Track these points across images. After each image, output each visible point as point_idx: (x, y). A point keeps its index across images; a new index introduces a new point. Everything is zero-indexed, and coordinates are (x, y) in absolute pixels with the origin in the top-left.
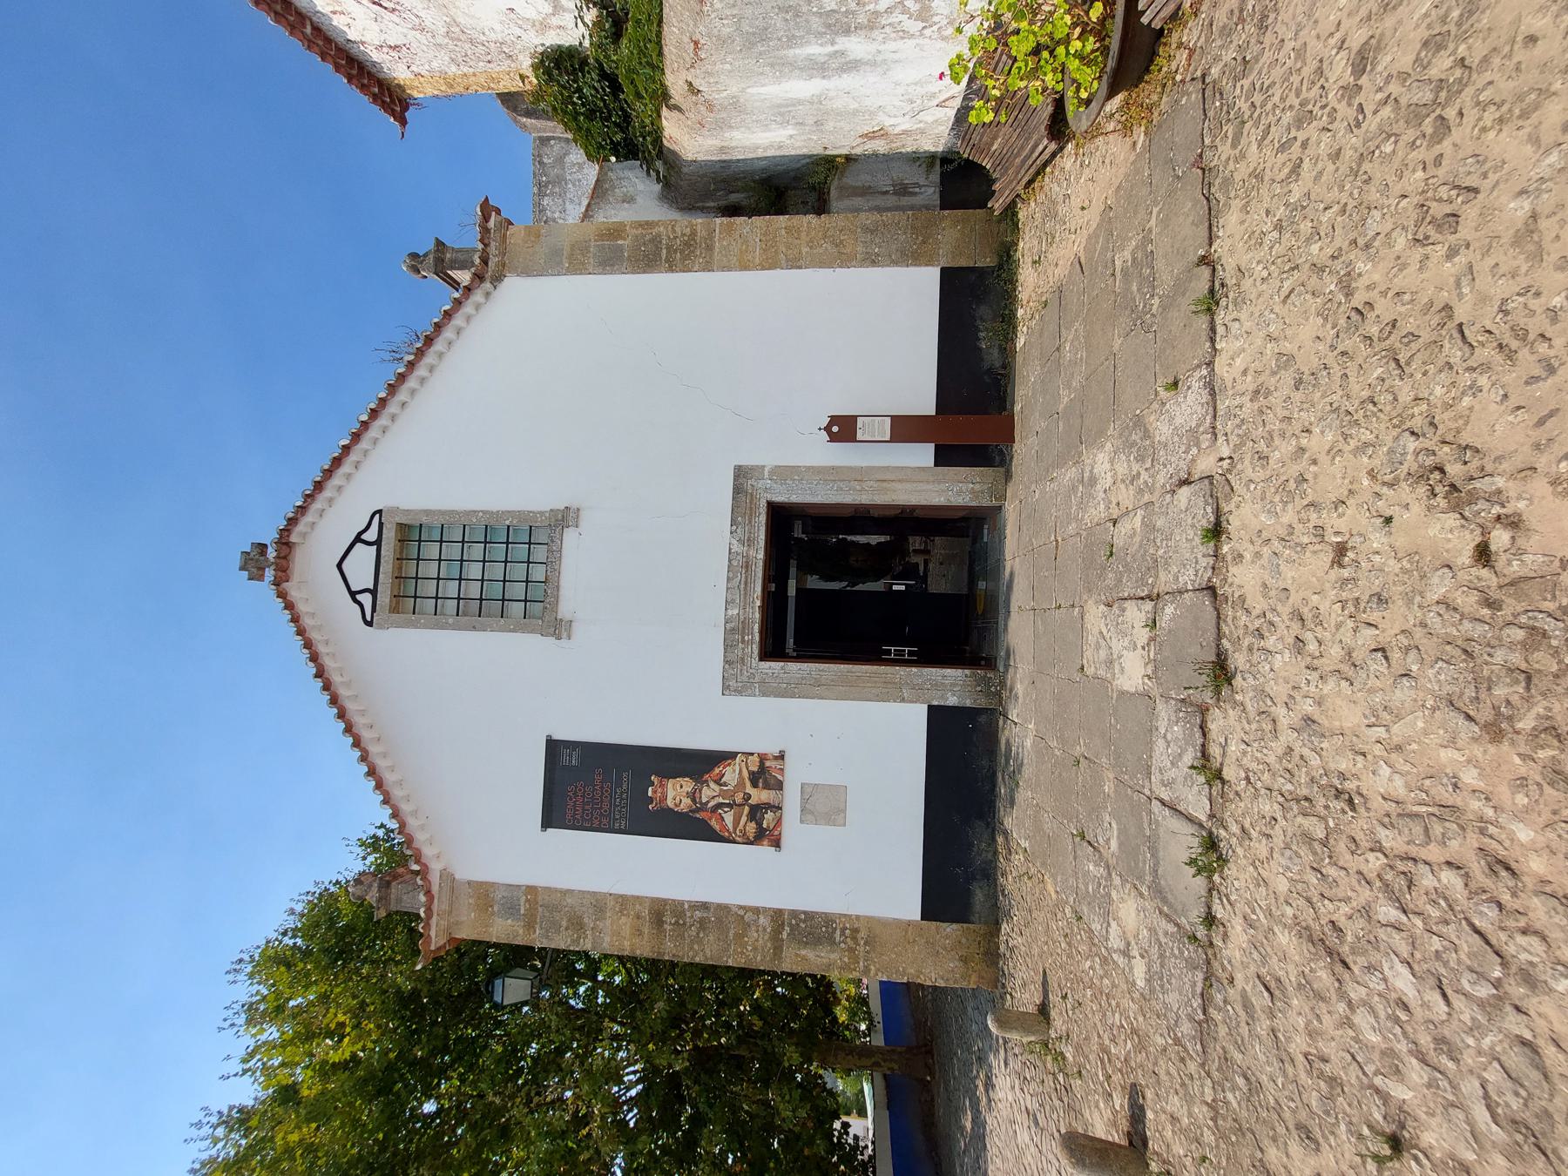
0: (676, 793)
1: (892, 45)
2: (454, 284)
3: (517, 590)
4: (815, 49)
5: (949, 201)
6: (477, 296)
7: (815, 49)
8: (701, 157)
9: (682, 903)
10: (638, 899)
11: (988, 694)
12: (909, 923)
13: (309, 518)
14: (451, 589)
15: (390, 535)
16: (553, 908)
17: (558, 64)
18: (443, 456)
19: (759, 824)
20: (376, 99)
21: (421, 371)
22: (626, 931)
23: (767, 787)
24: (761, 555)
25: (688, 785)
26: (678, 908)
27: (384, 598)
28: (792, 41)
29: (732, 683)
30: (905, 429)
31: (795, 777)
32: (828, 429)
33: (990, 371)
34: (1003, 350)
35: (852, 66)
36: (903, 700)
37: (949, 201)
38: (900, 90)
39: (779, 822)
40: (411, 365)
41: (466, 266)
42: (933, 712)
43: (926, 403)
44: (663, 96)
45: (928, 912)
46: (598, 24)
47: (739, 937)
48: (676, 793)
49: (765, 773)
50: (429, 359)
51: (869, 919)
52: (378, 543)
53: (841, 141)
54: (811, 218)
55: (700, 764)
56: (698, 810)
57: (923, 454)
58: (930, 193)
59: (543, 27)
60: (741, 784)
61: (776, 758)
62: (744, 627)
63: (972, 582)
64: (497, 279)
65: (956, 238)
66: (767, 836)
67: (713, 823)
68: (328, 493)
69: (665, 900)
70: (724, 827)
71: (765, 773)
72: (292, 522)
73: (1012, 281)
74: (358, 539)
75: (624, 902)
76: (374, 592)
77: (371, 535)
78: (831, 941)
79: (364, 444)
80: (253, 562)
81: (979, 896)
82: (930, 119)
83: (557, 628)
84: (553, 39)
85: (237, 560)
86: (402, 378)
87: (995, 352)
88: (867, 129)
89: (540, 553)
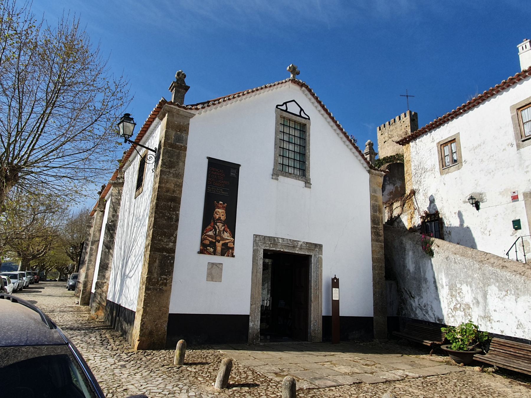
0: (220, 213)
3: (286, 162)
9: (179, 211)
15: (303, 121)
18: (325, 143)
24: (296, 252)
25: (223, 218)
26: (177, 208)
27: (285, 114)
29: (258, 239)
30: (336, 304)
36: (251, 305)
38: (429, 303)
39: (210, 254)
43: (343, 312)
48: (220, 213)
49: (228, 250)
52: (300, 116)
55: (231, 223)
56: (214, 221)
57: (325, 310)
60: (224, 239)
61: (233, 254)
64: (369, 172)
67: (210, 227)
69: (180, 204)
71: (228, 250)
74: (302, 110)
77: (303, 115)
83: (276, 174)
89: (297, 172)
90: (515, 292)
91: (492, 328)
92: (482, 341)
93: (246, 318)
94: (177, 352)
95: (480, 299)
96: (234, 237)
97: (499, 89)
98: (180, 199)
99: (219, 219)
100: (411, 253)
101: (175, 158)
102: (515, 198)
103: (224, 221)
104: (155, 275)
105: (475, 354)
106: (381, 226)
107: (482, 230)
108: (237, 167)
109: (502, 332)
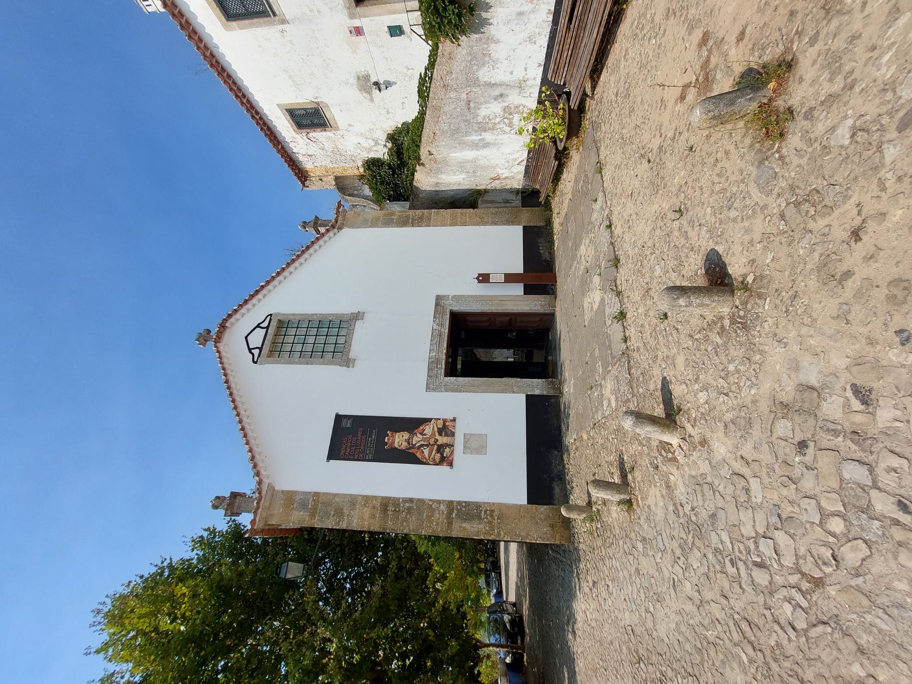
0: (399, 440)
1: (500, 137)
2: (318, 232)
3: (331, 348)
4: (474, 138)
5: (524, 205)
6: (326, 238)
7: (474, 138)
8: (429, 188)
9: (399, 499)
10: (375, 498)
11: (554, 389)
12: (521, 506)
13: (237, 316)
14: (299, 348)
15: (274, 324)
16: (327, 504)
17: (373, 164)
18: (301, 293)
19: (442, 455)
20: (296, 174)
21: (302, 260)
22: (366, 516)
23: (446, 435)
24: (447, 331)
25: (406, 435)
26: (396, 502)
27: (265, 351)
28: (467, 133)
30: (510, 278)
31: (460, 431)
32: (477, 278)
33: (545, 261)
34: (550, 253)
35: (487, 145)
37: (524, 205)
38: (504, 157)
39: (452, 453)
40: (299, 256)
41: (321, 228)
42: (529, 398)
43: (519, 268)
44: (418, 158)
45: (531, 500)
46: (390, 149)
47: (429, 517)
48: (399, 440)
49: (446, 429)
50: (306, 255)
51: (500, 505)
52: (267, 328)
53: (482, 182)
54: (471, 210)
55: (412, 425)
56: (410, 448)
57: (518, 289)
58: (518, 202)
59: (370, 150)
60: (433, 434)
61: (451, 421)
62: (438, 361)
63: (546, 358)
64: (340, 228)
65: (530, 216)
66: (445, 460)
67: (418, 455)
68: (249, 306)
69: (389, 498)
70: (424, 457)
71: (446, 429)
72: (225, 320)
73: (552, 228)
74: (258, 326)
75: (367, 499)
76: (261, 349)
77: (265, 325)
78: (479, 518)
79: (270, 287)
80: (204, 338)
81: (557, 490)
82: (515, 171)
83: (348, 363)
84: (372, 155)
85: (196, 336)
86: (293, 261)
87: (547, 254)
88: (493, 175)
89: (343, 332)
90: (485, 43)
91: (534, 79)
92: (553, 92)
93: (530, 399)
94: (573, 516)
95: (497, 92)
96: (429, 420)
97: (202, 46)
98: (383, 498)
99: (408, 441)
100: (443, 176)
101: (329, 509)
102: (358, 31)
103: (410, 433)
104: (481, 526)
105: (569, 107)
106: (411, 213)
107: (407, 79)
108: (339, 418)
109: (540, 65)
